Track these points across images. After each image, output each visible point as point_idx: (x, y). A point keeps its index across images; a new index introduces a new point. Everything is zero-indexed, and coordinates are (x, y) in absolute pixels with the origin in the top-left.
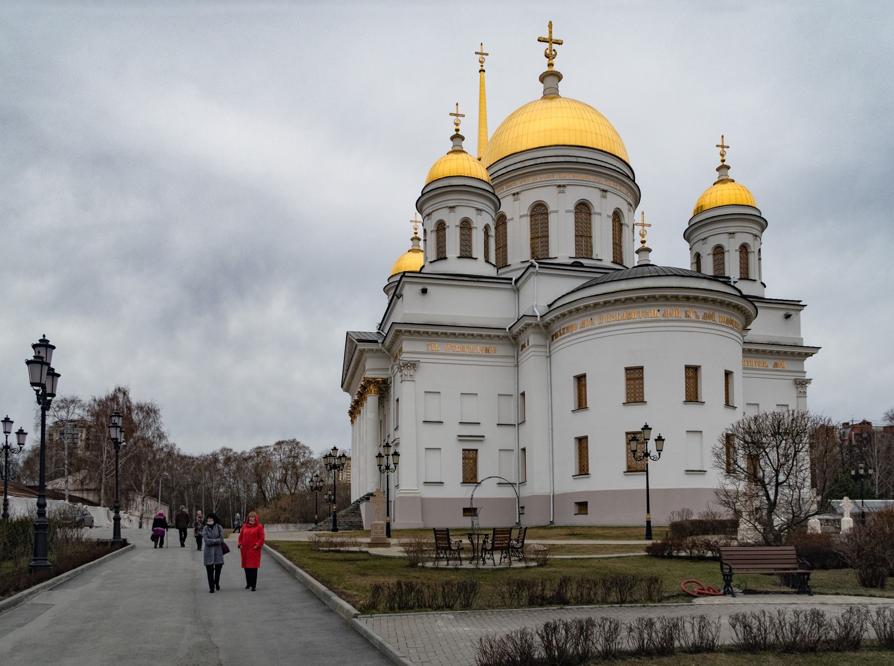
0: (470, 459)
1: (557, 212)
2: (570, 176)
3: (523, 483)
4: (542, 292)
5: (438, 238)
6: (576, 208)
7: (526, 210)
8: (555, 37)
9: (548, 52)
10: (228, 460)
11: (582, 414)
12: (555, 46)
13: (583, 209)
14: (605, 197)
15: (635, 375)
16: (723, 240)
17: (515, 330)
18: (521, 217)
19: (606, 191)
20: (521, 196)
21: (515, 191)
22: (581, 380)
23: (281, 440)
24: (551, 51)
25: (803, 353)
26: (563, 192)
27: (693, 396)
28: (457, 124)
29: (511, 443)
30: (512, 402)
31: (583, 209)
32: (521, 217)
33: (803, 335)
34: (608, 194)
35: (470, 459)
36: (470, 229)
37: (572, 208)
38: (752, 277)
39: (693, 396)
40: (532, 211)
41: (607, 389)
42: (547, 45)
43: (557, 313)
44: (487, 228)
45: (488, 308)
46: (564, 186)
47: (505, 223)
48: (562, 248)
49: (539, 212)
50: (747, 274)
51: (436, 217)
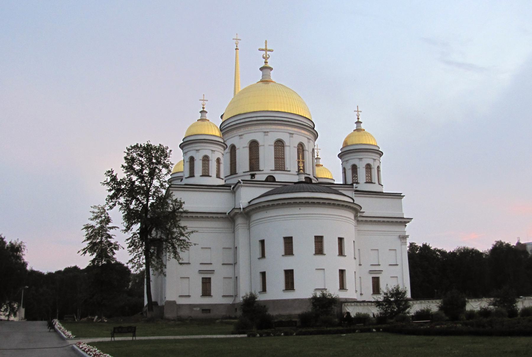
0: (206, 283)
2: (296, 130)
3: (235, 263)
4: (247, 195)
5: (190, 165)
6: (275, 143)
7: (247, 145)
8: (268, 48)
11: (263, 260)
12: (268, 53)
13: (279, 144)
14: (292, 137)
15: (288, 241)
16: (356, 162)
17: (232, 214)
19: (293, 134)
20: (243, 137)
21: (240, 134)
22: (262, 242)
24: (266, 55)
25: (403, 222)
26: (267, 135)
27: (319, 251)
28: (203, 105)
29: (231, 275)
30: (231, 252)
31: (279, 144)
32: (243, 148)
33: (404, 211)
34: (294, 136)
35: (206, 283)
36: (208, 161)
37: (273, 144)
38: (373, 181)
39: (319, 251)
40: (250, 145)
41: (275, 247)
42: (264, 52)
43: (254, 207)
44: (218, 160)
45: (217, 202)
46: (268, 132)
47: (235, 151)
48: (267, 164)
49: (254, 146)
50: (371, 179)
51: (190, 154)
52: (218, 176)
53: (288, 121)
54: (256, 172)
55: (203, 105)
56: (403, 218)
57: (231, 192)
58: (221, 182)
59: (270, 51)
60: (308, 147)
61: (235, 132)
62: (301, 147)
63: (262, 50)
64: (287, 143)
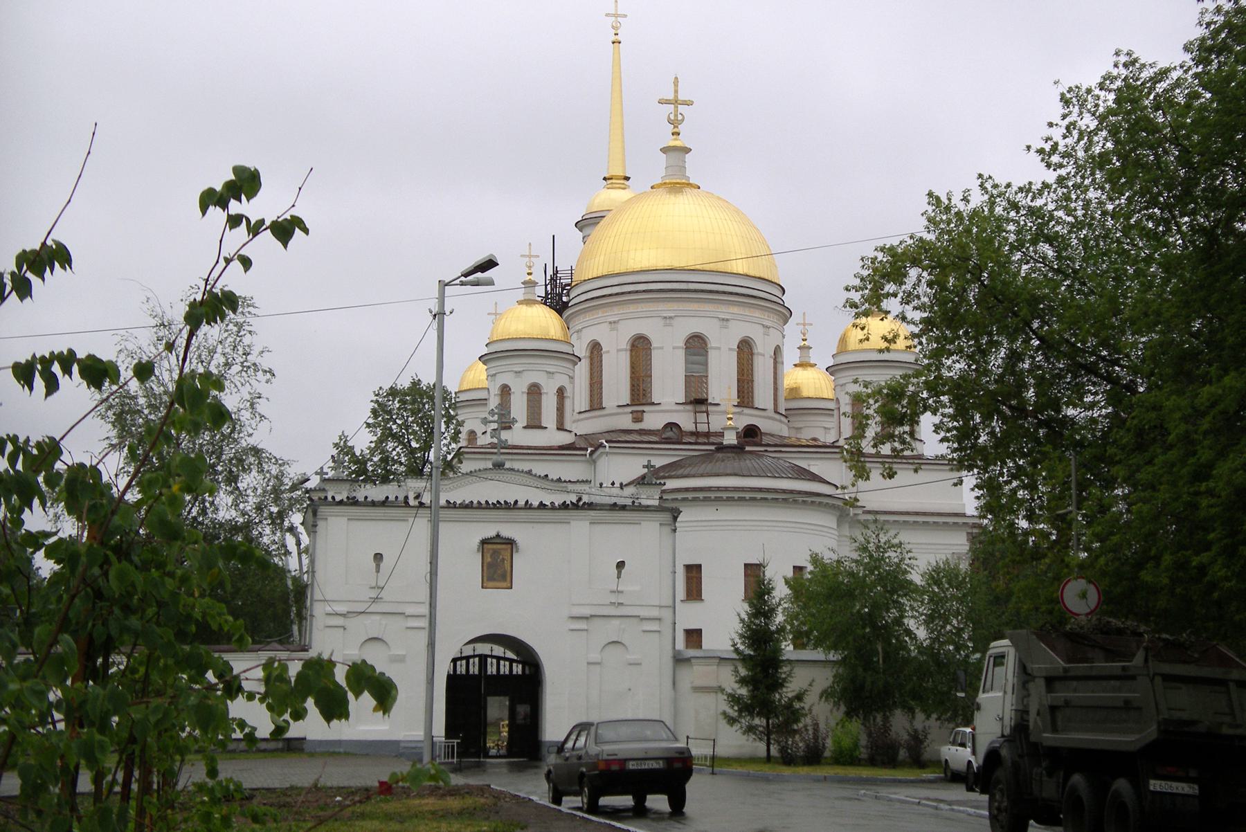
1: (662, 348)
7: (624, 343)
8: (681, 97)
9: (672, 117)
10: (241, 640)
18: (618, 351)
23: (584, 719)
24: (676, 116)
26: (670, 325)
28: (530, 267)
37: (682, 344)
48: (668, 387)
51: (503, 379)
52: (561, 428)
53: (717, 292)
54: (645, 408)
55: (530, 267)
56: (964, 515)
57: (587, 461)
58: (566, 439)
59: (685, 103)
60: (764, 348)
61: (600, 313)
62: (745, 349)
63: (667, 102)
64: (712, 343)
